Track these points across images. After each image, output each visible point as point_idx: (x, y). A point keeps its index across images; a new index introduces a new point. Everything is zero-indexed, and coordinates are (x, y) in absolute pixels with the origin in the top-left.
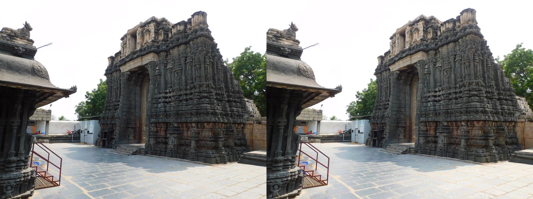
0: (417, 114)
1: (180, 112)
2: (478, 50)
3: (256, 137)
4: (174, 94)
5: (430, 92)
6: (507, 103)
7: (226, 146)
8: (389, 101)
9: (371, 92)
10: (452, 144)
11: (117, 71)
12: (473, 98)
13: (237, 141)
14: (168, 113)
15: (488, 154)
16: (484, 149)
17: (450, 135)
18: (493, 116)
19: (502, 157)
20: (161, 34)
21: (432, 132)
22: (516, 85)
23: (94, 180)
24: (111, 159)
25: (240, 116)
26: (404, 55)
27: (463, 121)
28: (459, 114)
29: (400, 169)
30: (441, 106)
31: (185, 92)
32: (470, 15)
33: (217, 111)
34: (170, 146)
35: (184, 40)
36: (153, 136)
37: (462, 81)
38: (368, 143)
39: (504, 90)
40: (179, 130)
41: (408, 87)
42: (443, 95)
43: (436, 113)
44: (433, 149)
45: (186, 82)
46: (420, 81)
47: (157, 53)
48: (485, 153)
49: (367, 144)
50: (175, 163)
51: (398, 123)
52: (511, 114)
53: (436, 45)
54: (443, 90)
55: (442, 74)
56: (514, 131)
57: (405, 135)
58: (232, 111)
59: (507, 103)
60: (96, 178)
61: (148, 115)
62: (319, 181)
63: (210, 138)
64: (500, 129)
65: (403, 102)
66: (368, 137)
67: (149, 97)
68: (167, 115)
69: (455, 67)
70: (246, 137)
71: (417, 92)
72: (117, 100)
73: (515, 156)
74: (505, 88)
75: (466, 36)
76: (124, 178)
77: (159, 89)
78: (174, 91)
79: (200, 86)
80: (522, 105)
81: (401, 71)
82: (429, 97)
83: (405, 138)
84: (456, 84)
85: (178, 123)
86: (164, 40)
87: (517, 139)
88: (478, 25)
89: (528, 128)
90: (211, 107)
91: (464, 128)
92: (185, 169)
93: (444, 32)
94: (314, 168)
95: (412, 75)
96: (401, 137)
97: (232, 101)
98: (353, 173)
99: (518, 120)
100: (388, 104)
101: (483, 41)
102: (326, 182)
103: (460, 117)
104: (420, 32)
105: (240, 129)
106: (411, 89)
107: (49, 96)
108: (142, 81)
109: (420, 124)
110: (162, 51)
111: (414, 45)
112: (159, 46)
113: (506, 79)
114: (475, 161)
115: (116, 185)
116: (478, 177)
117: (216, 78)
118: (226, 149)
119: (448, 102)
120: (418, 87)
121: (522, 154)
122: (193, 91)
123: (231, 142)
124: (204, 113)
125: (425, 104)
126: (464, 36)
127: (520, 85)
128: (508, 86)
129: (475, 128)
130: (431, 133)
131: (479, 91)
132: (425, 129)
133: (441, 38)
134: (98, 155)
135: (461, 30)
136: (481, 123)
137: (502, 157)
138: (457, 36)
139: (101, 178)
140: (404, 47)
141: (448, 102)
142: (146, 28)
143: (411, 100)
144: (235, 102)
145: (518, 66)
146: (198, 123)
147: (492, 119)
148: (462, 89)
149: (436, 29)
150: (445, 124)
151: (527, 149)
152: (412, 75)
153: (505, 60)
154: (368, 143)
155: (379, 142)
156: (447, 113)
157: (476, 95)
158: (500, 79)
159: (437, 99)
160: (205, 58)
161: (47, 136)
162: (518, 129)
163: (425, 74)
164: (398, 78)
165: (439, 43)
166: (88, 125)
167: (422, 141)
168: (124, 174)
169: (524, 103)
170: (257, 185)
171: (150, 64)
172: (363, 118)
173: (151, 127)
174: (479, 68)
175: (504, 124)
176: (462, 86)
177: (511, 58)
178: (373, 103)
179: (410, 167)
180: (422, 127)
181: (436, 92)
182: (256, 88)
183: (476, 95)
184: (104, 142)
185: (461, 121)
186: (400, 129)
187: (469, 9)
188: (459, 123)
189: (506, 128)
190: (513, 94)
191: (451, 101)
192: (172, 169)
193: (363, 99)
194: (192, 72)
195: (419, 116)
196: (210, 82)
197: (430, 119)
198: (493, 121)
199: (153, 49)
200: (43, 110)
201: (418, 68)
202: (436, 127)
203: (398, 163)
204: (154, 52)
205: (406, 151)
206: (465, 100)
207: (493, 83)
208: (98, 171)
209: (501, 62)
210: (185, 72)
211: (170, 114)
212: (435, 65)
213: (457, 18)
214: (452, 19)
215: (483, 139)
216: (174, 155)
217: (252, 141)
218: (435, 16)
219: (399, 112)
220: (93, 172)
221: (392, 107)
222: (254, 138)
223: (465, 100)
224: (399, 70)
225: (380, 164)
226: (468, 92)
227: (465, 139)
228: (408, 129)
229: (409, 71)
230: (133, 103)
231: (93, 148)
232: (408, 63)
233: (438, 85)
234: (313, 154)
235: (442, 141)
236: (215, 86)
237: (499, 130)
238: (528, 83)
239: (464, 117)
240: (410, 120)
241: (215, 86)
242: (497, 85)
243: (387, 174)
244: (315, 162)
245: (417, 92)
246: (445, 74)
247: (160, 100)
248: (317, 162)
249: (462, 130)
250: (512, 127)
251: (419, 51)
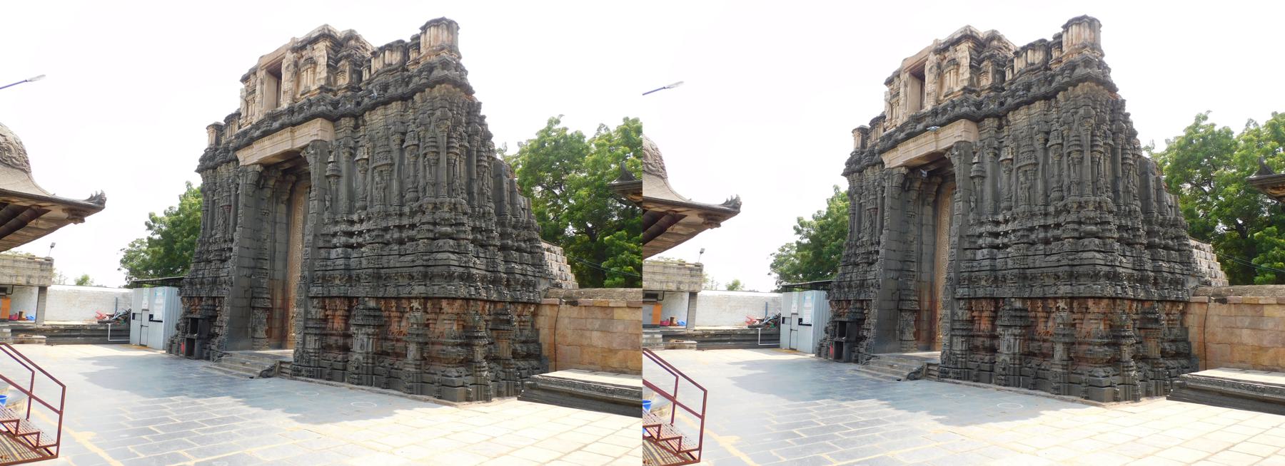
0: (303, 277)
1: (382, 271)
2: (1104, 121)
3: (1213, 334)
5: (336, 223)
6: (1168, 255)
7: (1140, 358)
8: (879, 243)
9: (836, 220)
10: (1032, 354)
11: (874, 165)
12: (1086, 241)
13: (1166, 345)
14: (354, 273)
15: (1118, 379)
16: (1108, 369)
17: (1028, 329)
18: (487, 289)
19: (504, 389)
20: (986, 72)
21: (985, 325)
22: (1190, 214)
23: (153, 442)
24: (206, 388)
25: (529, 285)
26: (276, 125)
27: (416, 298)
28: (406, 281)
29: (898, 419)
30: (364, 258)
31: (397, 222)
32: (1086, 34)
33: (1121, 270)
34: (1003, 357)
35: (1043, 90)
36: (314, 331)
37: (1062, 198)
38: (175, 347)
39: (1161, 225)
40: (380, 316)
41: (928, 210)
42: (1014, 231)
43: (351, 277)
44: (340, 366)
46: (313, 194)
47: (332, 118)
48: (1111, 379)
49: (819, 355)
50: (1013, 399)
51: (901, 300)
52: (1177, 283)
53: (1002, 104)
54: (1015, 219)
55: (369, 178)
56: (1182, 324)
57: (918, 330)
58: (1158, 270)
59: (1168, 255)
60: (802, 442)
61: (949, 279)
62: (35, 448)
63: (455, 338)
64: (502, 321)
65: (268, 245)
66: (175, 332)
67: (307, 232)
68: (350, 277)
69: (401, 163)
70: (1190, 335)
71: (305, 223)
72: (875, 239)
73: (1182, 387)
74: (517, 222)
75: (1075, 85)
76: (232, 437)
77: (980, 214)
78: (370, 219)
79: (436, 207)
80: (1204, 262)
81: (267, 167)
82: (980, 236)
83: (918, 339)
84: (402, 205)
85: (1024, 299)
86: (350, 88)
87: (540, 345)
88: (1105, 59)
89: (1216, 318)
90: (1105, 259)
91: (418, 314)
92: (390, 414)
93: (1021, 73)
94: (21, 414)
95: (939, 180)
96: (909, 335)
97: (1159, 246)
98: (131, 427)
99: (1194, 299)
100: (231, 249)
101: (473, 103)
102: (53, 450)
103: (408, 289)
104: (318, 70)
105: (1176, 317)
106: (936, 215)
107: (671, 224)
108: (292, 191)
109: (955, 304)
110: (344, 116)
111: (303, 100)
112: (338, 102)
113: (1169, 198)
114: (1087, 398)
115: (852, 458)
116: (445, 437)
117: (1121, 188)
118: (492, 365)
119: (1027, 249)
120: (309, 208)
121: (1197, 380)
122: (416, 219)
123: (504, 349)
124: (1087, 275)
125: (969, 254)
126: (1069, 84)
127: (1201, 213)
128: (1171, 215)
129: (1089, 316)
130: (336, 325)
131: (456, 225)
132: (967, 316)
133: (1013, 87)
134: (173, 378)
135: (420, 72)
136: (1104, 303)
137: (1152, 389)
138: (411, 86)
139: (816, 439)
140: (278, 105)
141: (1027, 249)
142: (307, 53)
143: (934, 244)
144: (1166, 248)
145: (1198, 166)
146: (426, 299)
147: (484, 295)
148: (416, 219)
149: (358, 66)
150: (372, 304)
151: (562, 369)
152: (939, 180)
153: (1169, 150)
154: (175, 347)
155: (851, 350)
156: (378, 277)
157: (1095, 235)
158: (1153, 196)
159: (999, 241)
160: (1093, 135)
161: (39, 326)
162: (1192, 320)
163: (328, 177)
164: (258, 182)
165: (1009, 100)
166: (152, 299)
167: (312, 344)
168: (234, 427)
169: (1209, 256)
170: (559, 455)
171: (957, 149)
172: (814, 287)
173: (310, 308)
174: (1105, 166)
175: (510, 308)
177: (1181, 148)
178: (840, 247)
179: (278, 410)
180: (313, 311)
181: (352, 223)
182: (1220, 214)
183: (1095, 235)
184: (190, 342)
185: (1055, 299)
186: (906, 316)
187: (1085, 17)
188: (1051, 304)
189: (1164, 316)
190: (1184, 233)
191: (387, 249)
192: (1005, 416)
193: (813, 238)
194: (1061, 170)
195: (309, 281)
196: (1104, 197)
197: (334, 292)
198: (1133, 300)
199: (965, 109)
200: (31, 259)
201: (955, 161)
202: (996, 311)
203: (250, 400)
204: (965, 116)
206: (422, 245)
207: (1137, 206)
208: (167, 420)
209: (1158, 156)
210: (399, 170)
211: (1004, 276)
212: (997, 155)
213: (1055, 38)
214: (401, 42)
215: (460, 345)
216: (1011, 381)
217: (1204, 345)
218: (359, 32)
219: (903, 271)
220: (797, 426)
221: (887, 259)
222: (558, 339)
223: (422, 245)
225: (203, 402)
226: (431, 227)
227: (1065, 343)
228: (925, 316)
229: (287, 166)
230: (914, 247)
231: (163, 359)
232: (931, 148)
233: (357, 205)
234: (21, 375)
235: (362, 346)
236: (1119, 206)
237: (500, 323)
238: (1220, 209)
239: (418, 290)
240: (285, 291)
241: (1119, 206)
242: (1146, 210)
243: (864, 431)
244: (27, 397)
245: (305, 223)
246: (1022, 179)
248: (31, 397)
249: (1059, 321)
250: (529, 317)
251: (313, 117)
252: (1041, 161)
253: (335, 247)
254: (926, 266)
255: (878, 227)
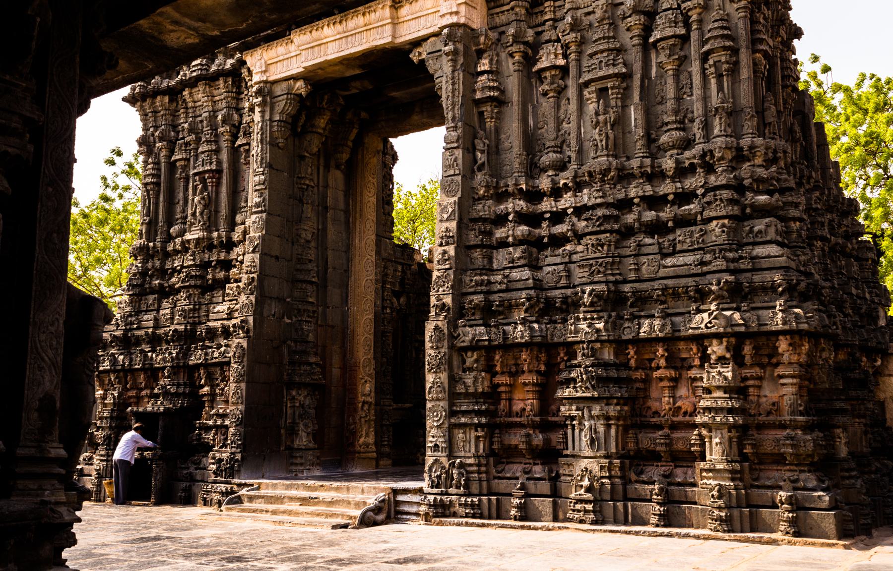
4: (586, 197)
31: (648, 190)
40: (629, 381)
45: (650, 140)
59: (849, 266)
176: (692, 169)
205: (377, 510)
224: (309, 76)
227: (731, 427)
232: (381, 38)
247: (500, 233)
252: (637, 67)
253: (503, 244)
254: (334, 295)
255: (224, 211)
